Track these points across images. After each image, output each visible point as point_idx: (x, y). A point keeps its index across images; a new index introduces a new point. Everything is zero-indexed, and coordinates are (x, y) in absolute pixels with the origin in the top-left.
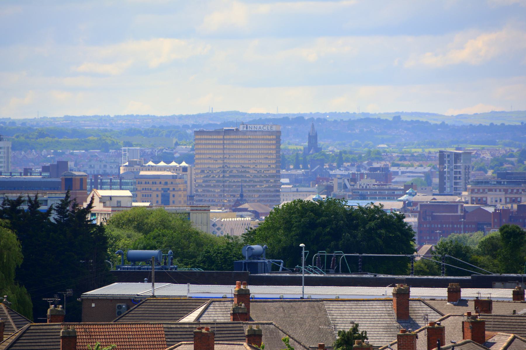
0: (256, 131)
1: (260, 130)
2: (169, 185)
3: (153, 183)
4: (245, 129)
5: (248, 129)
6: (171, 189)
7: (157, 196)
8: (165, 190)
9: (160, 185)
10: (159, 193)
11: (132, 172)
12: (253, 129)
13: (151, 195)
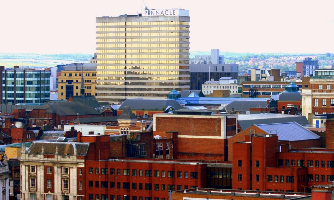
0: (158, 16)
1: (162, 15)
2: (72, 77)
3: (93, 74)
4: (147, 14)
5: (150, 15)
6: (75, 81)
7: (62, 87)
8: (70, 82)
9: (65, 77)
10: (64, 85)
11: (156, 74)
12: (155, 15)
13: (90, 87)
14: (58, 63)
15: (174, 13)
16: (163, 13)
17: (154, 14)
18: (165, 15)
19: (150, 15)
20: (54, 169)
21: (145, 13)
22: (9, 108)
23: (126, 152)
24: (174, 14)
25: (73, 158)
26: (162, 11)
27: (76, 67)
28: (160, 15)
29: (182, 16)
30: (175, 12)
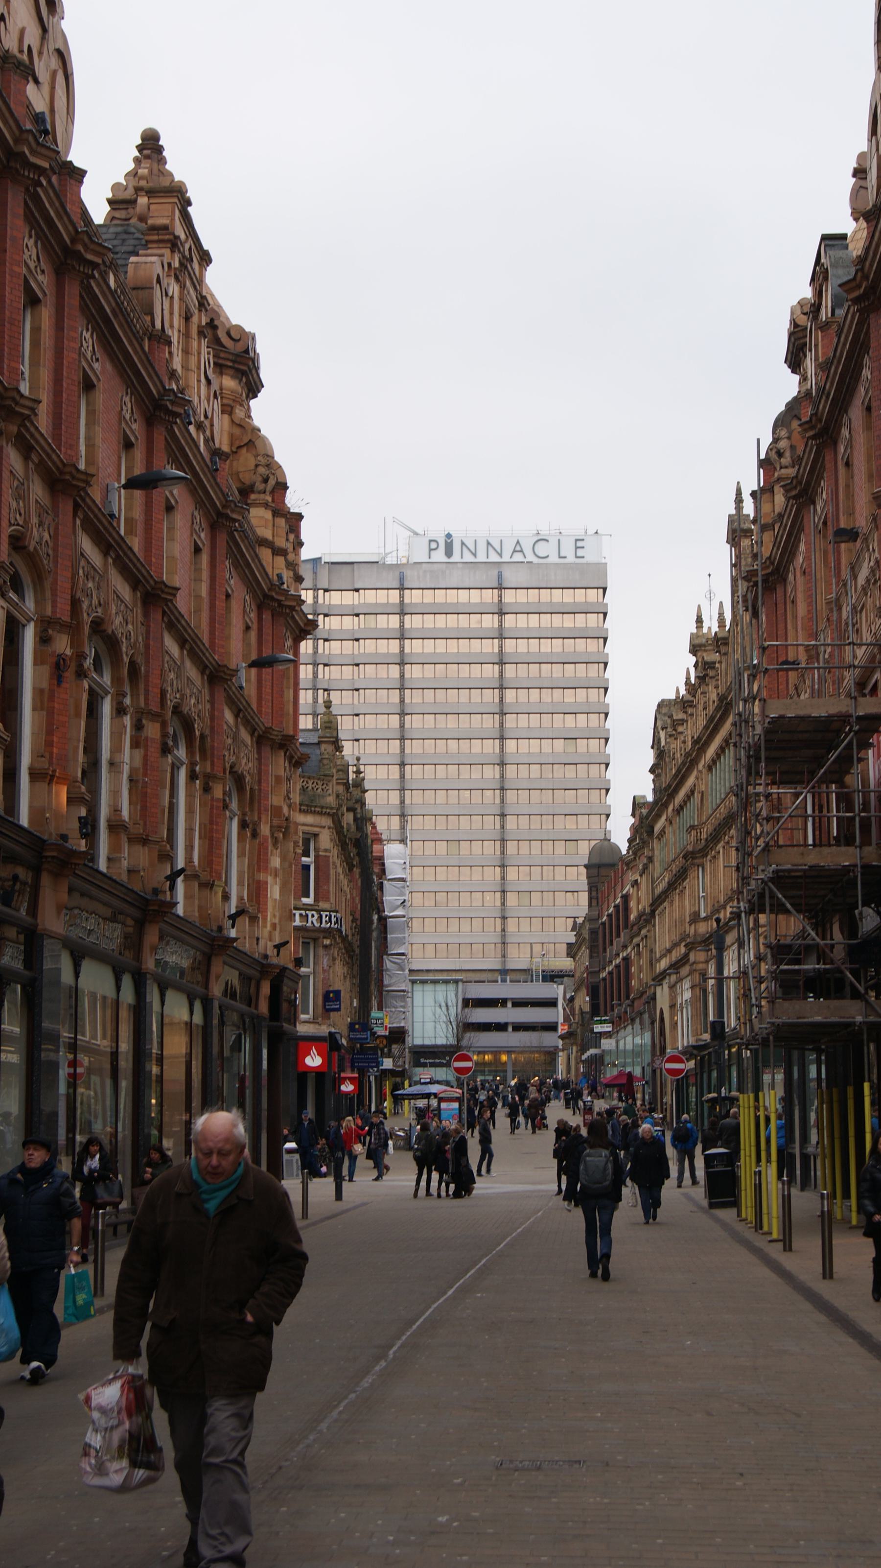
1: (518, 557)
5: (456, 558)
12: (481, 557)
14: (688, 669)
15: (580, 553)
16: (521, 551)
17: (475, 555)
18: (531, 557)
19: (452, 560)
20: (222, 1109)
21: (431, 550)
23: (96, 1174)
24: (579, 554)
26: (518, 542)
28: (508, 560)
30: (583, 547)
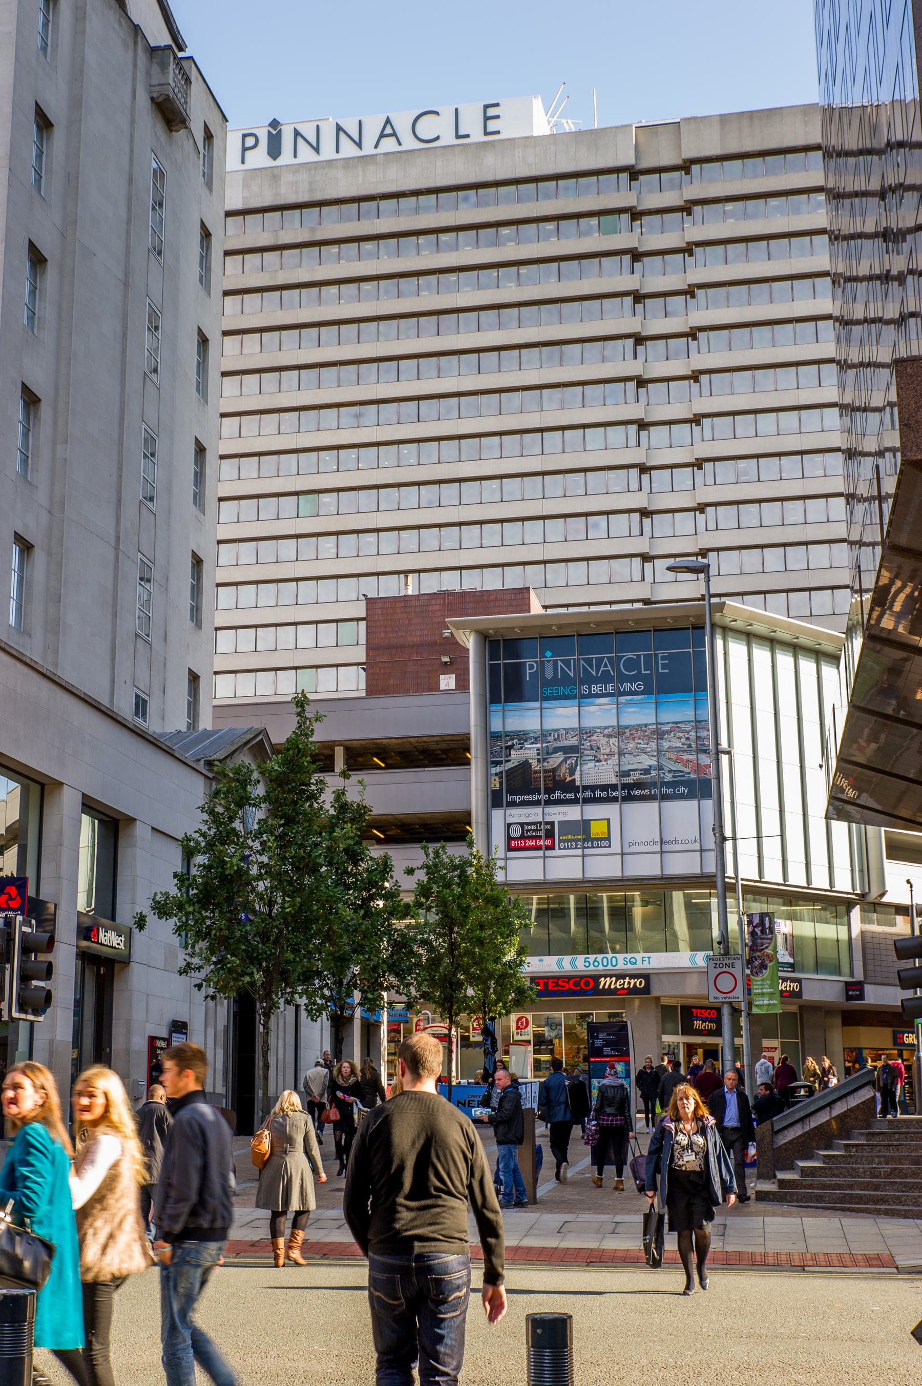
5: (286, 157)
16: (394, 134)
21: (245, 149)
22: (215, 1049)
24: (489, 130)
25: (620, 765)
26: (388, 121)
27: (605, 353)
29: (388, 153)
